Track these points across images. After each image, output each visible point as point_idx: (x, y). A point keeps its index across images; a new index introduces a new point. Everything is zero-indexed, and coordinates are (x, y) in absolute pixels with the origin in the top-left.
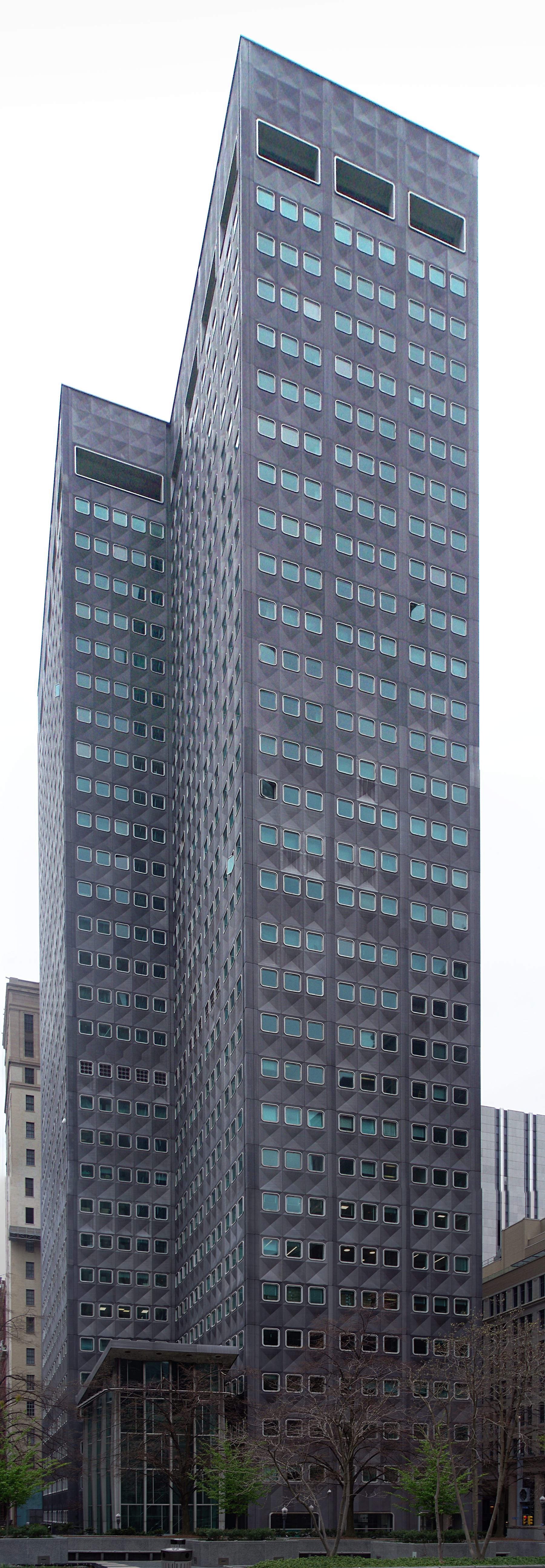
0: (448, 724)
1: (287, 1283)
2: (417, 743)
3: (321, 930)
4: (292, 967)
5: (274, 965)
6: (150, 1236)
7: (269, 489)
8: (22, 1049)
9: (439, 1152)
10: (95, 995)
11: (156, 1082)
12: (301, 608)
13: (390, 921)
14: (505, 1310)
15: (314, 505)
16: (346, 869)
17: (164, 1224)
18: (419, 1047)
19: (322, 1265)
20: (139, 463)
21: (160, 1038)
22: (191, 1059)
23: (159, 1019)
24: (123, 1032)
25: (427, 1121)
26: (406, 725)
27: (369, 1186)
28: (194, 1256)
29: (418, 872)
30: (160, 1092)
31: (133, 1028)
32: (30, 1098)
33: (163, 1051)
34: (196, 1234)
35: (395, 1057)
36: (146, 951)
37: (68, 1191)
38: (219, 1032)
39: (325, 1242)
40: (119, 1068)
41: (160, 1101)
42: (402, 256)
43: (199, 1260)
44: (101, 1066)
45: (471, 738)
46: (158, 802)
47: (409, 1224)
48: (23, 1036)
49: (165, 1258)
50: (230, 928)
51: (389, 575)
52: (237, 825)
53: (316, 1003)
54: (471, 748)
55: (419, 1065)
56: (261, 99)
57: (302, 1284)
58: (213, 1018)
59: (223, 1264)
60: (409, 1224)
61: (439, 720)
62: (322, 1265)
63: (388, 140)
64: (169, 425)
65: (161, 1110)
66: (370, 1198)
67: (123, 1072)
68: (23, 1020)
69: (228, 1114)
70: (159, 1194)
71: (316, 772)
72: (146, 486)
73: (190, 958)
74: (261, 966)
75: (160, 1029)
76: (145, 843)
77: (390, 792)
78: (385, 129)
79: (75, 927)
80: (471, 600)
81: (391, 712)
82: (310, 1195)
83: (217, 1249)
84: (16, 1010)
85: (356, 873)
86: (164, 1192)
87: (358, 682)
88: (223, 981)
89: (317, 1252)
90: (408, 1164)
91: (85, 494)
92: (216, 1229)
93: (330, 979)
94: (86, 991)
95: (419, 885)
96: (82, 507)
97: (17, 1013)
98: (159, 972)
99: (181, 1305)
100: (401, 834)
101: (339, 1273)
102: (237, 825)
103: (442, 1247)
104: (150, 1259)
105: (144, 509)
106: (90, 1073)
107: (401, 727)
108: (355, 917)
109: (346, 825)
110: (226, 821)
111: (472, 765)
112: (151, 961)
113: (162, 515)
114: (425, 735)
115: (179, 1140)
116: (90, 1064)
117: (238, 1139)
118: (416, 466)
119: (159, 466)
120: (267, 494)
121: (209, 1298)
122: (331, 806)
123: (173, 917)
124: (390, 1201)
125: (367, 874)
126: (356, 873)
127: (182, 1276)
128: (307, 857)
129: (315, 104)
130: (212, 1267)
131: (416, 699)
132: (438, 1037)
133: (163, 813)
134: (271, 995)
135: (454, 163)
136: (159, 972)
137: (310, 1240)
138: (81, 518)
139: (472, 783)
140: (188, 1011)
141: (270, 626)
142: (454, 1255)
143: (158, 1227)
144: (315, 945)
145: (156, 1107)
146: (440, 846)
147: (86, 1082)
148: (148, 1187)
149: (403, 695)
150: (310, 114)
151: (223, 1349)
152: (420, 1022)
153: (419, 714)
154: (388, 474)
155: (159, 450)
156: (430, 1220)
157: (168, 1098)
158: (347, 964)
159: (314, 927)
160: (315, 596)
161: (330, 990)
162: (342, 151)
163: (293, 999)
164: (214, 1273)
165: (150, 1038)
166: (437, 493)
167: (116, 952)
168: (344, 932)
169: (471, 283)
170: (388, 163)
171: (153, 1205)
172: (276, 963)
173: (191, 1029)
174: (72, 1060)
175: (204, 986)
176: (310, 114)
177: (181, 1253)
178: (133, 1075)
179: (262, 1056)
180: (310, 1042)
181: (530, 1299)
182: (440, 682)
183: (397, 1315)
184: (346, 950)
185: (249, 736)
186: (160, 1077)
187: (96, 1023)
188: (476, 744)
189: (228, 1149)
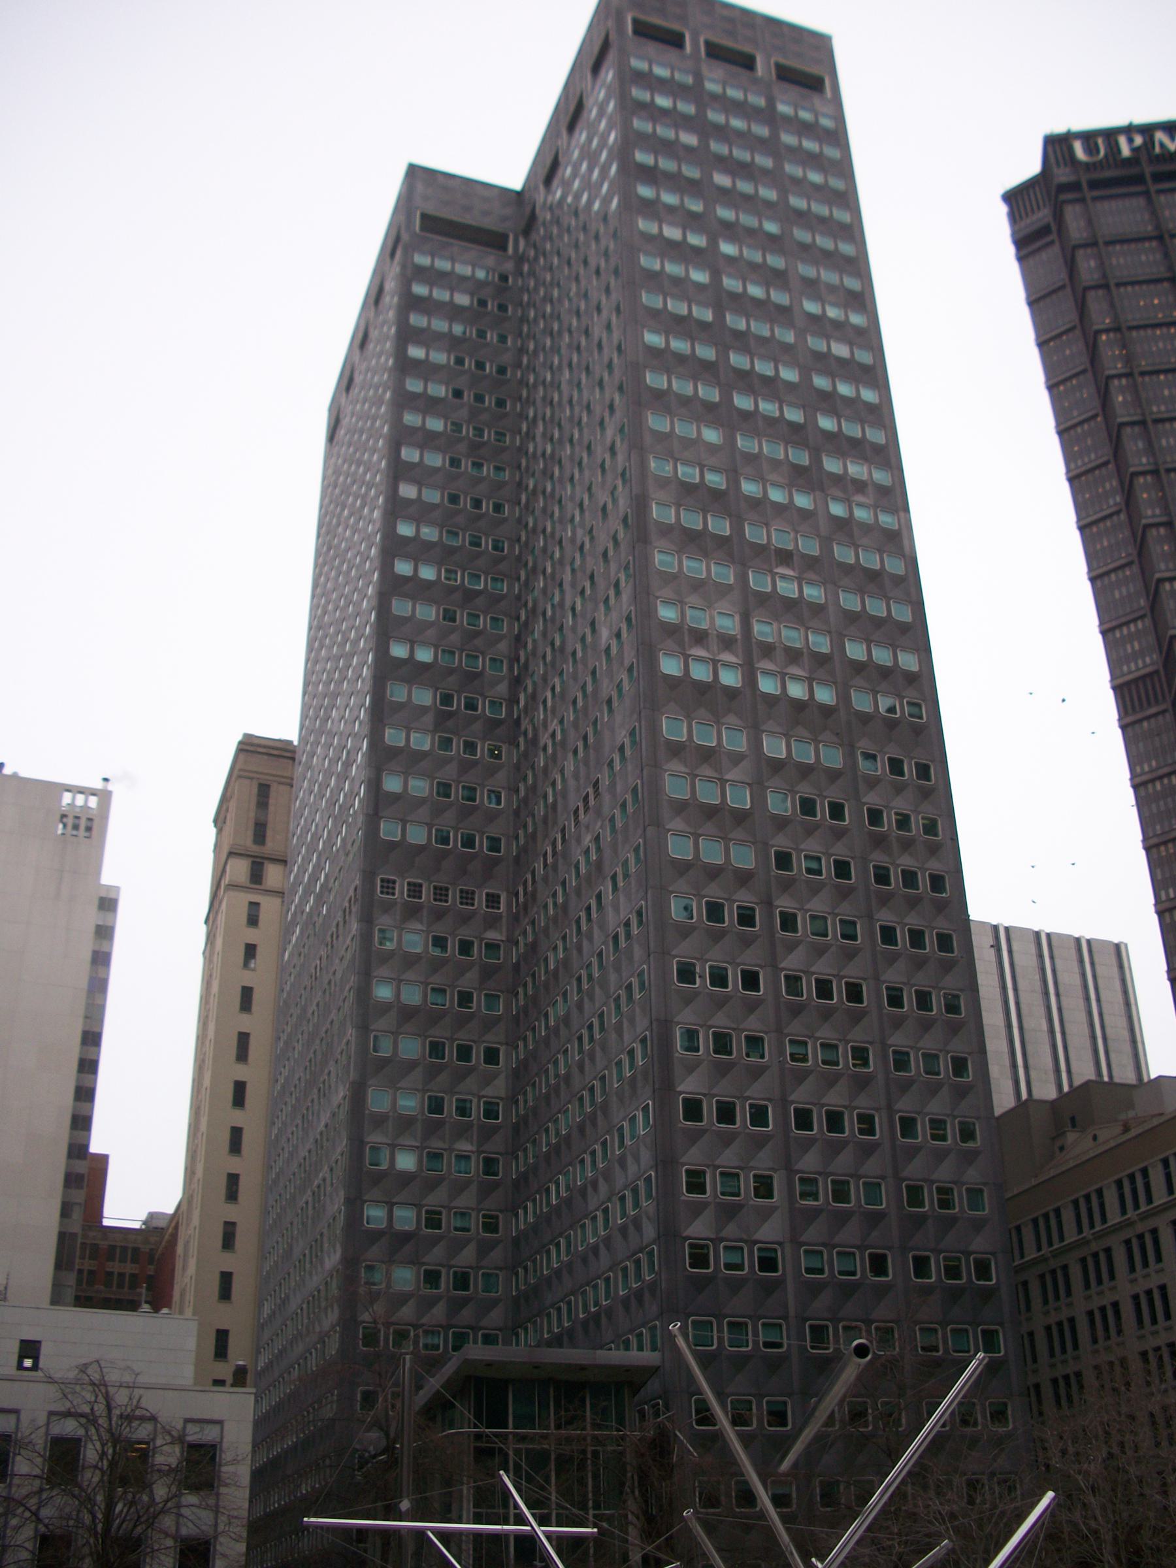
0: (870, 489)
1: (722, 1240)
2: (837, 509)
3: (739, 722)
4: (706, 770)
5: (683, 769)
6: (474, 1149)
8: (250, 834)
9: (926, 1026)
11: (487, 907)
12: (695, 378)
13: (827, 711)
14: (1022, 1257)
16: (768, 650)
17: (496, 1129)
18: (882, 877)
19: (772, 1210)
20: (488, 223)
21: (495, 844)
22: (545, 879)
25: (905, 980)
26: (823, 490)
27: (831, 1081)
28: (553, 1188)
29: (855, 651)
30: (492, 922)
31: (456, 830)
32: (254, 905)
33: (496, 862)
34: (557, 1149)
35: (851, 890)
36: (477, 726)
37: (353, 1075)
38: (599, 849)
39: (775, 1170)
40: (435, 888)
41: (492, 935)
43: (563, 1194)
44: (409, 884)
47: (893, 1138)
48: (252, 815)
49: (497, 1185)
50: (618, 718)
52: (625, 597)
53: (741, 817)
54: (902, 514)
55: (885, 900)
57: (745, 1242)
58: (587, 827)
59: (614, 1207)
60: (893, 1138)
61: (860, 486)
62: (772, 1210)
65: (492, 947)
66: (835, 1098)
67: (441, 893)
68: (255, 791)
69: (618, 970)
70: (488, 1080)
71: (722, 542)
72: (494, 241)
73: (545, 739)
74: (666, 771)
75: (494, 830)
77: (811, 563)
81: (802, 478)
82: (749, 1098)
83: (601, 1181)
84: (245, 777)
85: (779, 654)
86: (495, 1076)
88: (605, 782)
89: (764, 1187)
90: (885, 1046)
92: (598, 1147)
93: (758, 786)
95: (859, 668)
96: (422, 260)
97: (247, 782)
99: (526, 1269)
100: (831, 609)
101: (800, 1219)
102: (625, 597)
103: (944, 1173)
104: (474, 1188)
105: (490, 261)
106: (393, 894)
107: (817, 493)
109: (763, 599)
110: (608, 589)
111: (905, 533)
112: (484, 739)
113: (509, 266)
115: (521, 996)
116: (394, 882)
117: (638, 1010)
121: (585, 1260)
123: (516, 682)
124: (864, 1103)
125: (793, 656)
126: (779, 654)
127: (528, 1216)
128: (718, 636)
130: (591, 1207)
131: (832, 465)
132: (906, 861)
133: (503, 559)
134: (680, 807)
135: (820, 45)
137: (753, 1168)
140: (540, 810)
142: (964, 1184)
143: (487, 1134)
144: (738, 742)
145: (486, 944)
146: (878, 623)
147: (387, 908)
148: (472, 1070)
151: (615, 1356)
152: (879, 841)
153: (839, 480)
156: (923, 1130)
157: (504, 929)
158: (777, 766)
159: (732, 719)
161: (759, 800)
163: (711, 812)
164: (594, 1218)
165: (482, 844)
166: (829, 276)
168: (770, 725)
171: (480, 1098)
172: (686, 766)
173: (546, 836)
174: (369, 876)
175: (572, 783)
177: (524, 1178)
178: (453, 896)
179: (673, 892)
180: (737, 871)
181: (1062, 1239)
183: (888, 1287)
184: (775, 747)
185: (641, 504)
186: (493, 900)
189: (620, 1024)
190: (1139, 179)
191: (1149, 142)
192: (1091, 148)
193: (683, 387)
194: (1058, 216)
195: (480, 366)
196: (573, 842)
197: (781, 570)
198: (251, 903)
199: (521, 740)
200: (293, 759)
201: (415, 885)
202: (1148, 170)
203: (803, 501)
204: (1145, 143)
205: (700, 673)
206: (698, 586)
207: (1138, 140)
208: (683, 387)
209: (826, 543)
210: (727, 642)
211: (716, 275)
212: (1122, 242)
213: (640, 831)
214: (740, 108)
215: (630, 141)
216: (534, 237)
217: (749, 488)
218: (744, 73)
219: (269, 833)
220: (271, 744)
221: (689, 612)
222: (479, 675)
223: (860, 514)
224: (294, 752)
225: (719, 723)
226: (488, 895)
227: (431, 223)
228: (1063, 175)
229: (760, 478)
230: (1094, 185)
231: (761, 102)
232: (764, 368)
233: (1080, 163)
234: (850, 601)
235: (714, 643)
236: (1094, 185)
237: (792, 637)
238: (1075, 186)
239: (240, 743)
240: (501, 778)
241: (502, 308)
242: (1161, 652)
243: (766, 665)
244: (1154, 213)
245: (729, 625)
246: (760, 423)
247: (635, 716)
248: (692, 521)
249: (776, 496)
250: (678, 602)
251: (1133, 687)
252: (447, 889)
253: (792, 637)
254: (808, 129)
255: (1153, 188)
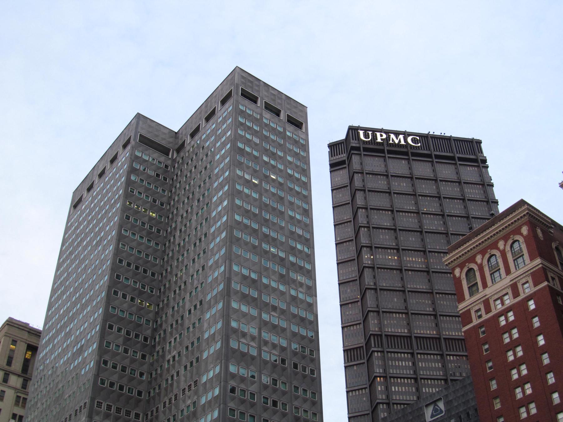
0: (304, 287)
2: (293, 293)
3: (255, 369)
7: (240, 192)
8: (6, 361)
10: (110, 365)
15: (255, 200)
16: (266, 343)
20: (163, 143)
23: (141, 382)
24: (121, 388)
33: (140, 401)
36: (139, 345)
42: (285, 129)
45: (314, 294)
46: (153, 274)
51: (282, 228)
54: (314, 297)
56: (242, 82)
61: (301, 285)
63: (281, 99)
64: (176, 133)
67: (118, 410)
72: (165, 151)
75: (140, 388)
76: (145, 292)
77: (283, 312)
78: (279, 96)
79: (105, 329)
80: (311, 241)
81: (282, 278)
85: (270, 345)
87: (269, 265)
91: (141, 149)
94: (105, 363)
96: (139, 154)
97: (8, 338)
98: (144, 357)
107: (287, 286)
108: (269, 365)
109: (266, 323)
111: (314, 304)
113: (169, 162)
114: (296, 290)
116: (102, 403)
118: (290, 193)
119: (171, 145)
120: (239, 193)
122: (260, 315)
123: (155, 330)
126: (270, 345)
129: (258, 86)
135: (303, 109)
136: (144, 357)
138: (137, 157)
139: (315, 312)
141: (238, 239)
147: (98, 413)
149: (288, 273)
150: (257, 88)
154: (281, 194)
155: (171, 140)
160: (255, 231)
162: (266, 98)
165: (135, 393)
166: (298, 202)
167: (124, 343)
169: (307, 140)
170: (281, 104)
176: (257, 88)
178: (123, 413)
182: (300, 270)
187: (108, 380)
188: (316, 296)
190: (382, 151)
191: (388, 138)
192: (366, 136)
193: (246, 238)
194: (349, 157)
195: (154, 201)
196: (181, 401)
197: (273, 313)
198: (2, 391)
199: (155, 354)
200: (40, 336)
201: (109, 405)
202: (386, 148)
203: (282, 288)
204: (387, 138)
205: (244, 349)
206: (245, 315)
207: (384, 136)
208: (246, 238)
209: (288, 305)
210: (253, 338)
211: (261, 195)
212: (373, 174)
213: (217, 405)
214: (273, 131)
215: (236, 138)
216: (182, 154)
217: (265, 281)
218: (276, 118)
219: (13, 362)
220: (23, 325)
221: (241, 325)
222: (141, 325)
223: (301, 296)
224: (40, 333)
225: (248, 368)
226: (136, 413)
227: (145, 141)
228: (354, 143)
229: (268, 277)
230: (365, 150)
231: (281, 129)
232: (273, 234)
233: (362, 140)
234: (295, 329)
235: (248, 338)
236: (365, 150)
237: (274, 339)
238: (358, 149)
239: (7, 321)
240: (145, 368)
241: (165, 179)
242: (365, 339)
243: (265, 348)
244: (386, 166)
245: (254, 332)
246: (270, 256)
247: (219, 361)
248: (246, 291)
249: (273, 284)
250: (237, 321)
251: (355, 351)
252: (121, 409)
253: (274, 339)
254: (296, 142)
255: (387, 156)
